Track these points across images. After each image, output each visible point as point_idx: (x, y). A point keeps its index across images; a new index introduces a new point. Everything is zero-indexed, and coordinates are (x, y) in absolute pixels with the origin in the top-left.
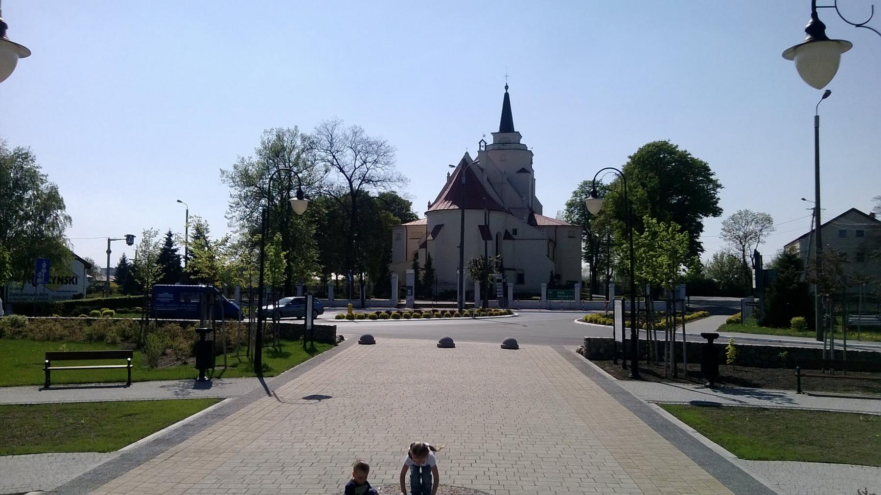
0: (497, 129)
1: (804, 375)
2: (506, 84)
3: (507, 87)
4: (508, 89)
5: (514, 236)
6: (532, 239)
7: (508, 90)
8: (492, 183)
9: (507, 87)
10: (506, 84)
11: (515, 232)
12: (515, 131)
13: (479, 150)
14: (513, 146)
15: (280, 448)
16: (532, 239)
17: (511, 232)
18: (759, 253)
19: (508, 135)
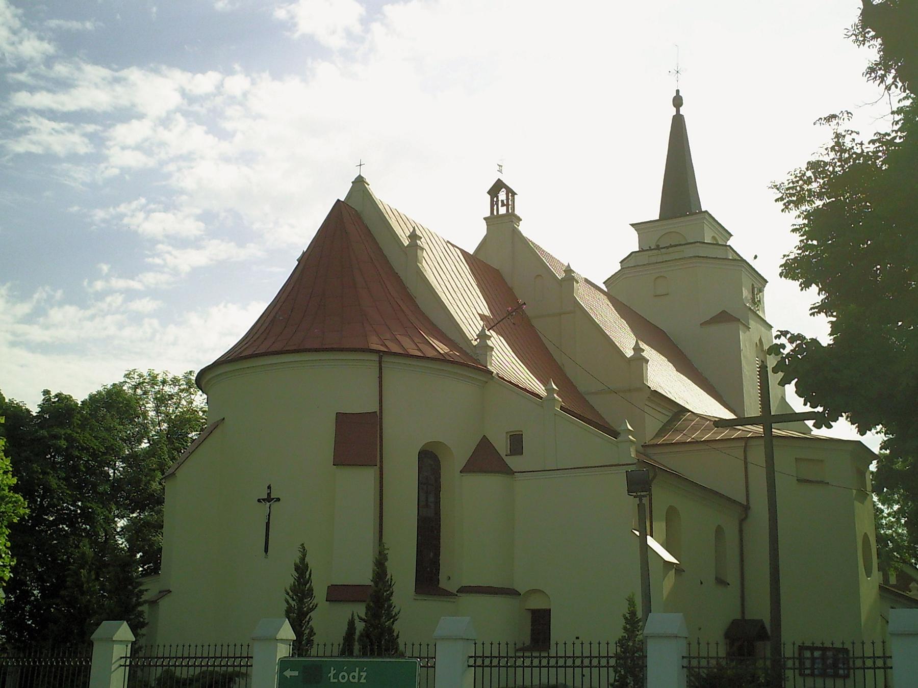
0: (652, 212)
1: (157, 655)
2: (678, 91)
3: (678, 101)
4: (681, 105)
5: (513, 462)
6: (689, 650)
7: (855, 134)
8: (749, 460)
9: (678, 101)
10: (678, 91)
11: (516, 443)
12: (703, 210)
13: (488, 214)
14: (689, 251)
15: (126, 382)
16: (689, 650)
17: (501, 445)
18: (674, 116)
19: (681, 226)
